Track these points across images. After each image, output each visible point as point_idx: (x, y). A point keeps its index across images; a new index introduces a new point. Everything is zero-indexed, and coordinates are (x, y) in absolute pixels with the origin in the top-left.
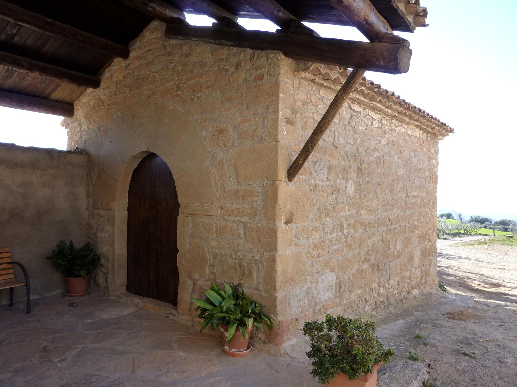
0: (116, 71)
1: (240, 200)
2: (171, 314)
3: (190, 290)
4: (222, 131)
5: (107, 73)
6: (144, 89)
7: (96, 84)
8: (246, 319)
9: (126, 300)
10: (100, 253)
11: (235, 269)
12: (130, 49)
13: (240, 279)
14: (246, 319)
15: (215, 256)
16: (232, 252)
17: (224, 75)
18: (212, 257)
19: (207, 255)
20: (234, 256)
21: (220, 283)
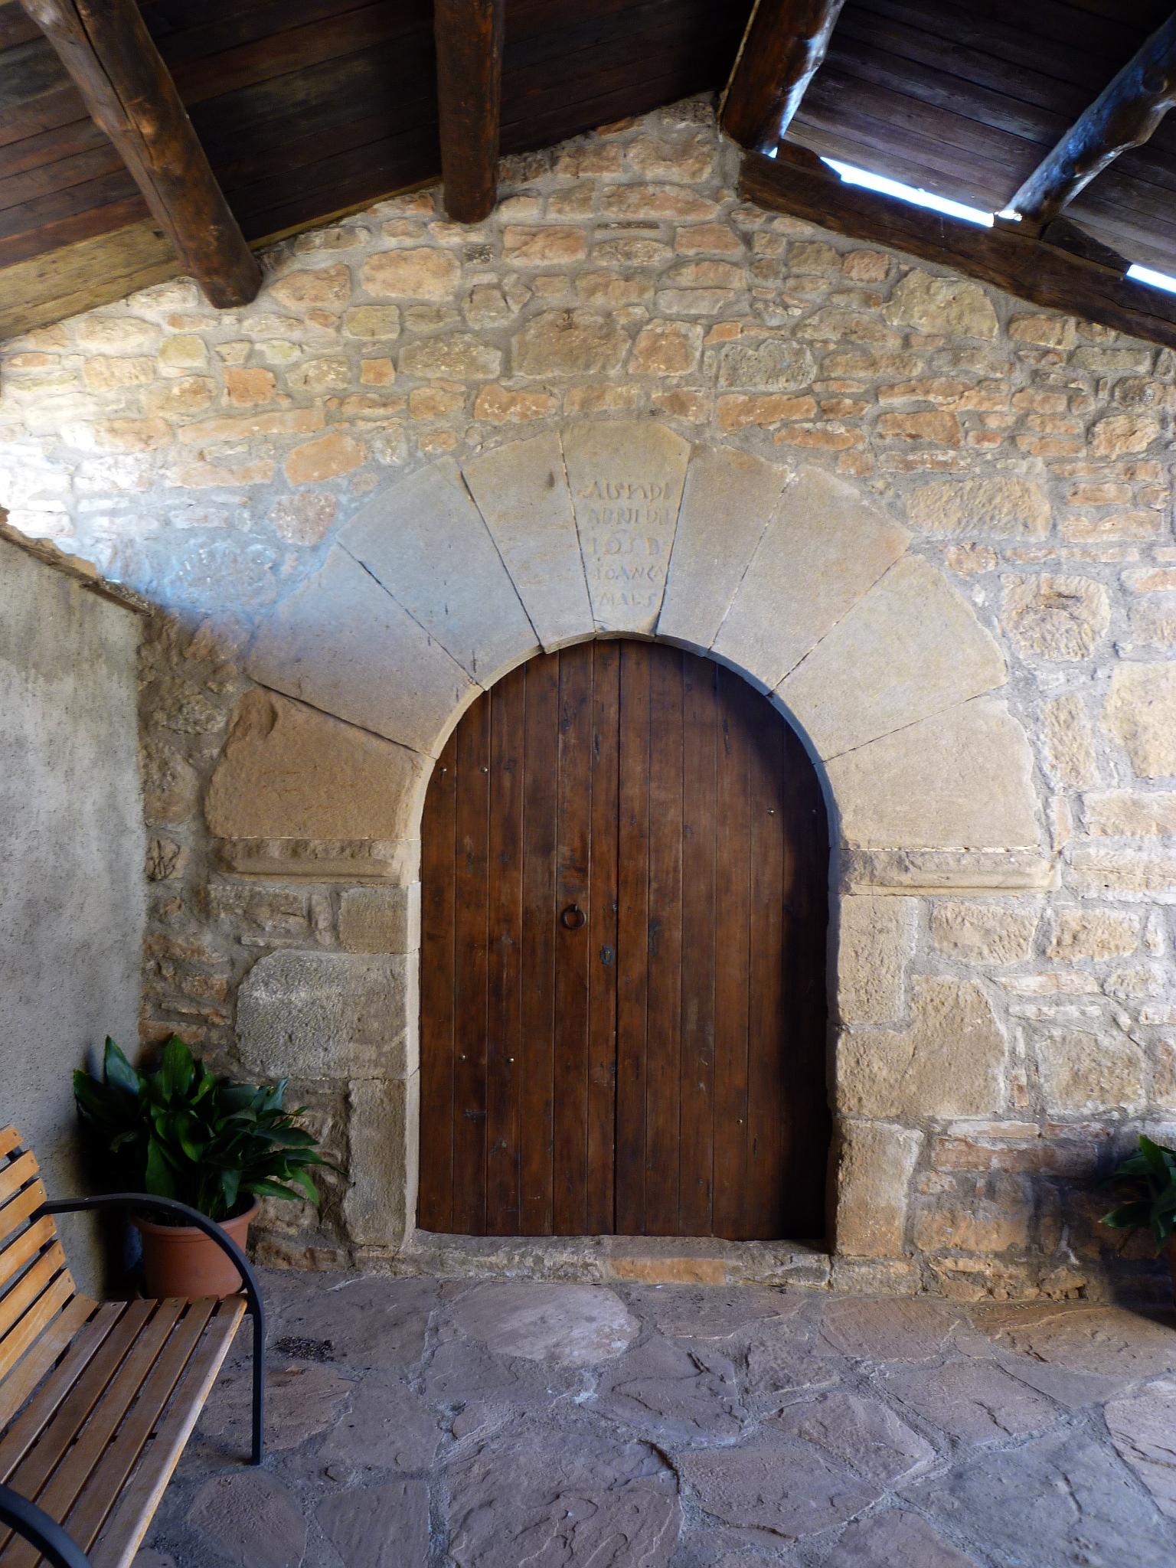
0: (392, 254)
1: (1153, 837)
2: (797, 1272)
3: (909, 1162)
4: (1063, 600)
5: (318, 254)
6: (613, 373)
7: (235, 281)
8: (201, 1148)
9: (491, 1267)
10: (270, 1087)
11: (1131, 1062)
12: (502, 189)
13: (1151, 1094)
14: (201, 1148)
15: (1032, 1028)
16: (1114, 1006)
17: (1061, 407)
18: (1019, 1033)
19: (1002, 1028)
20: (1125, 1020)
21: (1062, 1118)
